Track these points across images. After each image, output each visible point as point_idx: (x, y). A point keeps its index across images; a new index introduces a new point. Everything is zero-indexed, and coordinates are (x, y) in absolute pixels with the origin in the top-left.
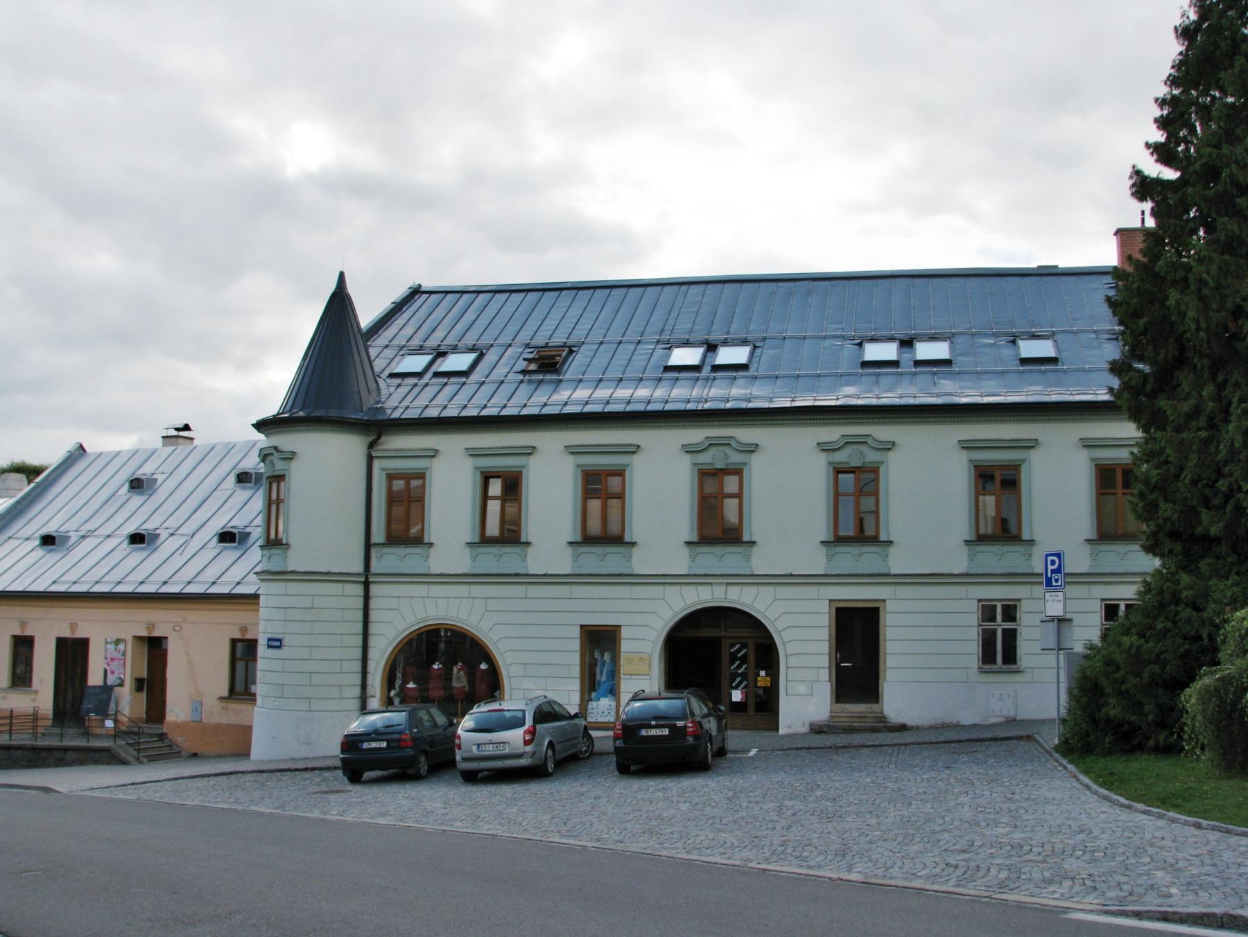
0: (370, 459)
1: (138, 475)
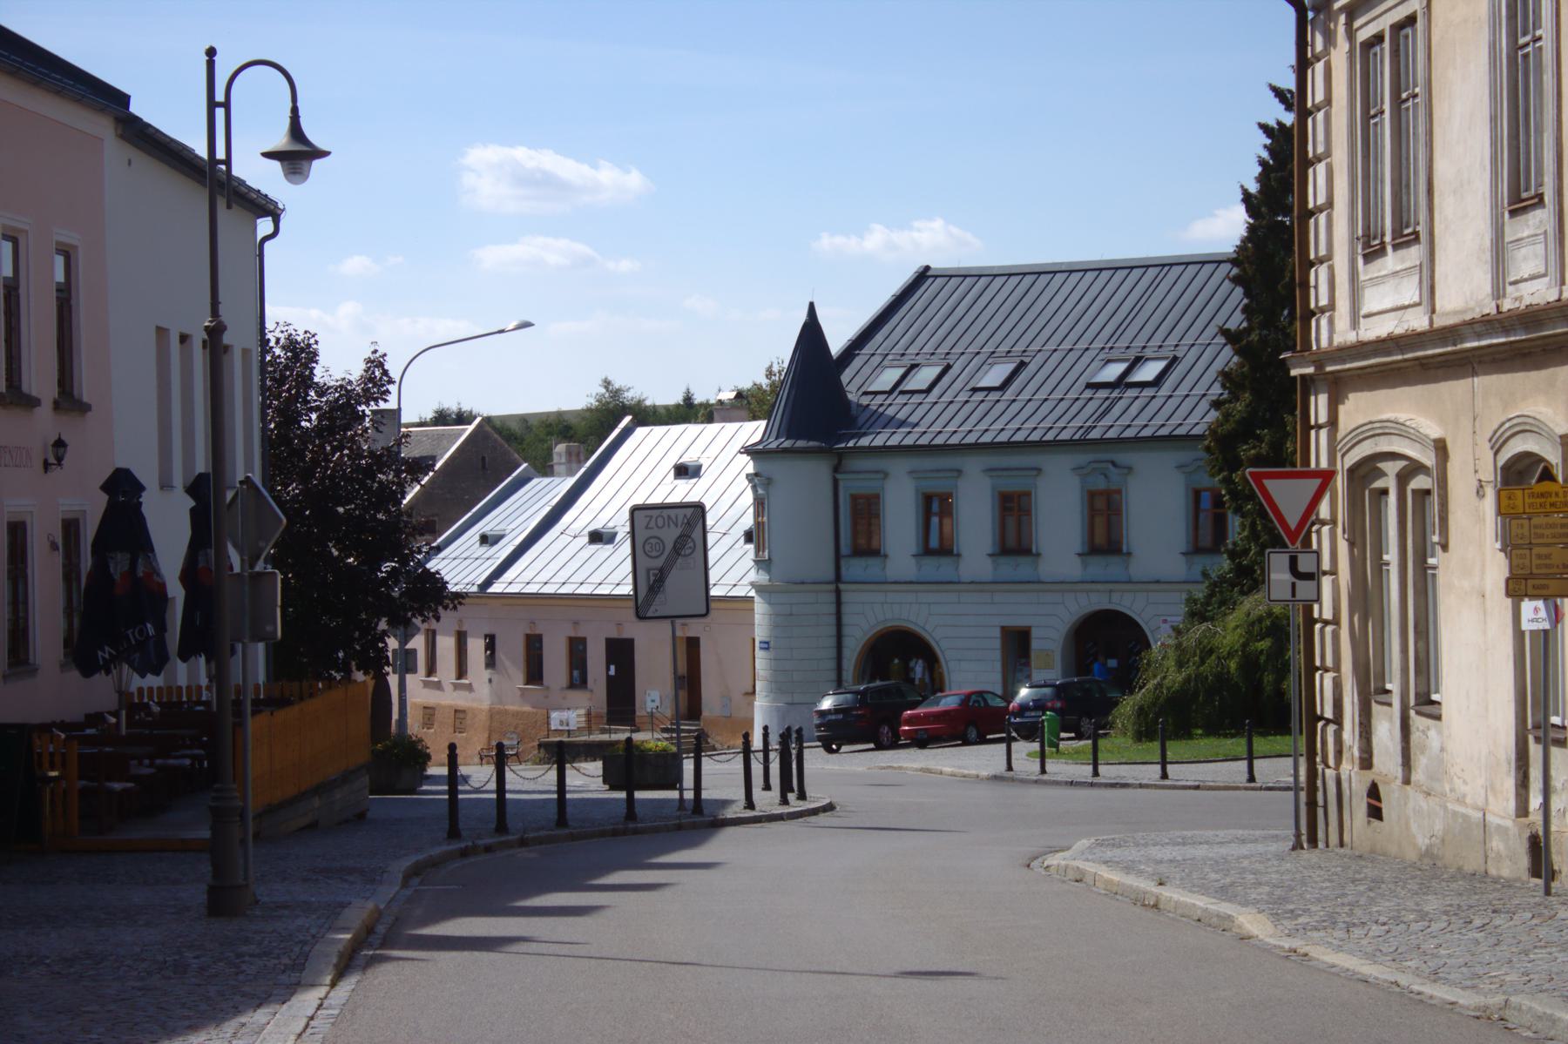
0: (836, 483)
1: (685, 459)
